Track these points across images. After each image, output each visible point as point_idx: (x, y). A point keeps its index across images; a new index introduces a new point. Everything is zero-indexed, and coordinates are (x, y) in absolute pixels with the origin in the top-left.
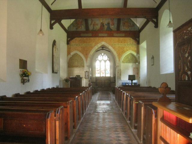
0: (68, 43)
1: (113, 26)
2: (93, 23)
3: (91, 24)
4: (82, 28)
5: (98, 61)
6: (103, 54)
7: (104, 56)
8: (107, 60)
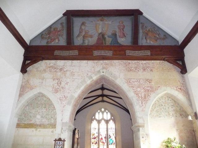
0: (24, 70)
1: (123, 39)
2: (83, 33)
3: (78, 36)
4: (59, 41)
5: (95, 120)
6: (103, 110)
7: (105, 113)
8: (110, 120)
